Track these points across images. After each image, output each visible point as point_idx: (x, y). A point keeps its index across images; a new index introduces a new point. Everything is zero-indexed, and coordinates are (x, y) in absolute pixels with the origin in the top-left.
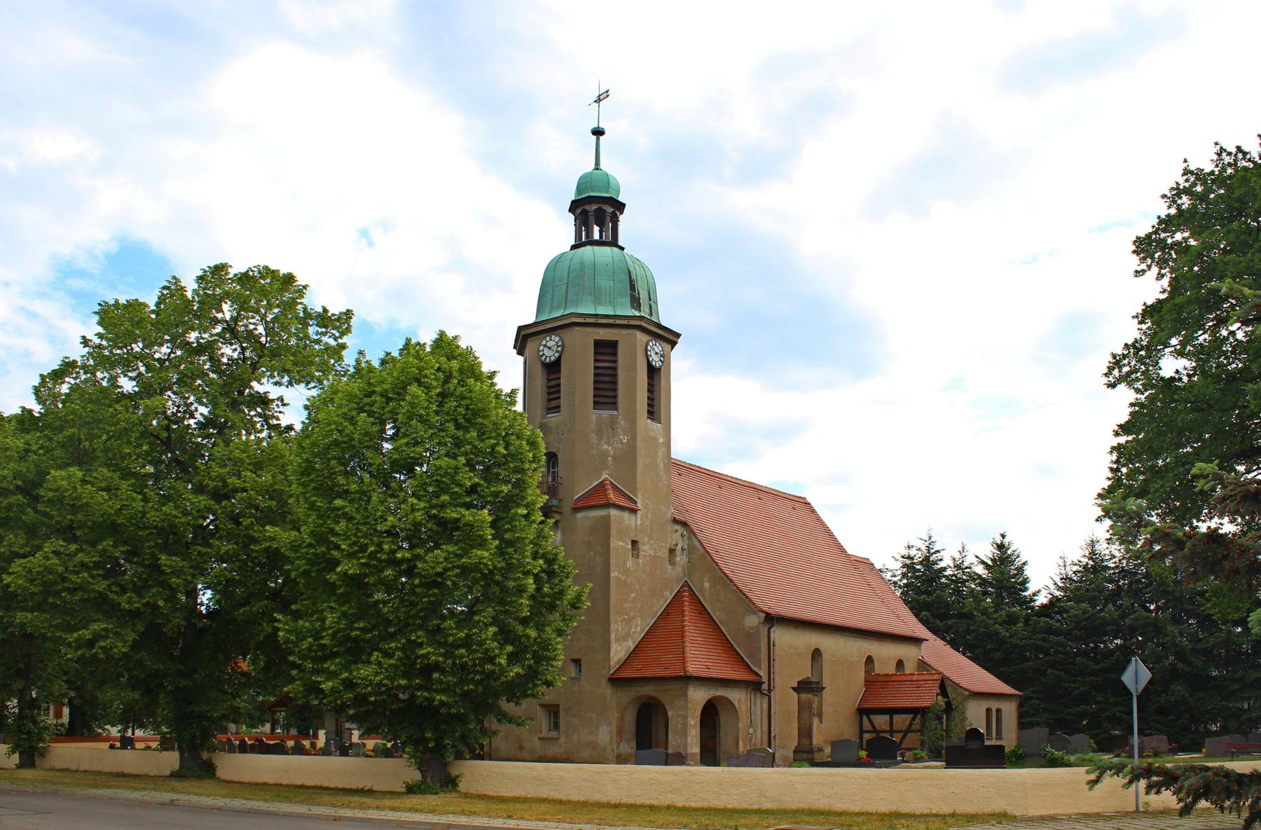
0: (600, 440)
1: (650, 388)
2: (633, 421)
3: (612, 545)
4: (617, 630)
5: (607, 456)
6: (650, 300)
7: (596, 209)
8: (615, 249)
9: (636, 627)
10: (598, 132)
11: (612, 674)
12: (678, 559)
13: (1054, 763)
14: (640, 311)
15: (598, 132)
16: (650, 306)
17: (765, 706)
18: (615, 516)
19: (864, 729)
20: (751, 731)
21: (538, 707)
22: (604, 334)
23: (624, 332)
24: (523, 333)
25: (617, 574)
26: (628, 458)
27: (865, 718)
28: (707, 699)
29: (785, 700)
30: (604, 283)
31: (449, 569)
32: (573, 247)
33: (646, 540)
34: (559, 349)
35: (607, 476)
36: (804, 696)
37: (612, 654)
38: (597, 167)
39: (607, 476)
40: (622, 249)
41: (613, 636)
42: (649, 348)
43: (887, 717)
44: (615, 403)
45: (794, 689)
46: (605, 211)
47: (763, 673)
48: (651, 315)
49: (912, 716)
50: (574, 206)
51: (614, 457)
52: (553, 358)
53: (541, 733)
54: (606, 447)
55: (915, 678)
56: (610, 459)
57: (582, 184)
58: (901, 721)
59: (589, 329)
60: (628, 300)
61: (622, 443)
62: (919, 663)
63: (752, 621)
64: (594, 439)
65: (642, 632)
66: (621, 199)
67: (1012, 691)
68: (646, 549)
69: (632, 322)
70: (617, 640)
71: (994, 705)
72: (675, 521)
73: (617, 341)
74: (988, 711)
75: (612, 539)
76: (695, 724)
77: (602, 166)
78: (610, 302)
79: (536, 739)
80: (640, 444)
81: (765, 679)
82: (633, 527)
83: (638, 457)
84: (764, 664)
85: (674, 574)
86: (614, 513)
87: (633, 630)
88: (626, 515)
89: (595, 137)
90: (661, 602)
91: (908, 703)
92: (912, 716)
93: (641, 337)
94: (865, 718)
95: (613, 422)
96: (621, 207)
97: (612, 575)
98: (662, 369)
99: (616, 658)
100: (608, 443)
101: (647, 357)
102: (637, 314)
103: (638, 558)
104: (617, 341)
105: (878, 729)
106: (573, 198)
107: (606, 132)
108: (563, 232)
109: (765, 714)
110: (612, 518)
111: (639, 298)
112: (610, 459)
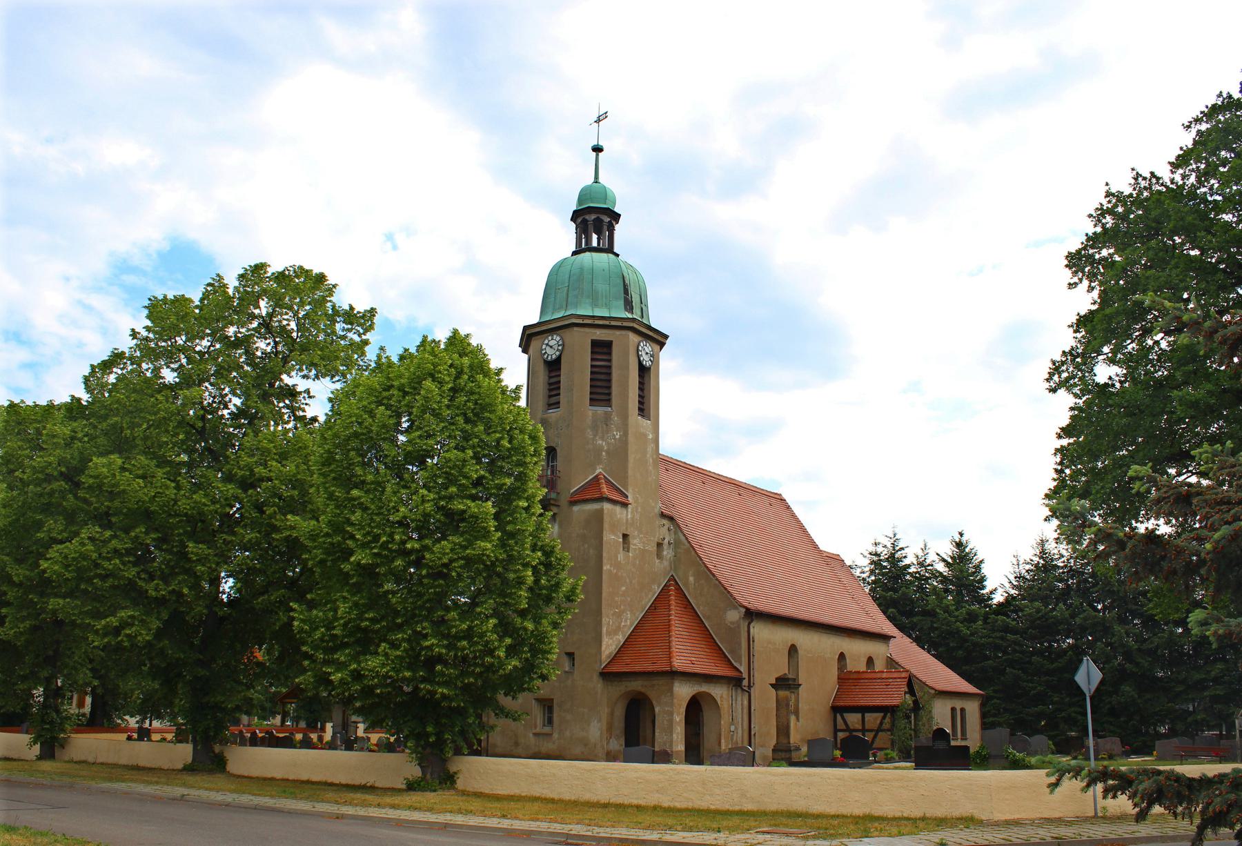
0: (595, 436)
1: (641, 406)
2: (625, 417)
3: (605, 539)
4: (608, 624)
8: (611, 256)
9: (626, 621)
10: (597, 149)
13: (1016, 765)
14: (632, 313)
15: (597, 149)
16: (642, 309)
17: (746, 702)
18: (608, 509)
20: (733, 728)
21: (534, 701)
23: (618, 333)
24: (528, 332)
26: (620, 453)
27: (838, 715)
29: (764, 697)
32: (574, 253)
34: (560, 348)
35: (601, 470)
36: (782, 693)
38: (596, 181)
39: (601, 470)
40: (617, 255)
41: (604, 630)
43: (859, 715)
46: (602, 221)
47: (744, 668)
48: (642, 317)
49: (882, 714)
50: (576, 216)
51: (608, 452)
52: (554, 357)
55: (884, 675)
56: (604, 453)
57: (584, 195)
59: (587, 330)
60: (622, 302)
61: (615, 439)
63: (734, 616)
65: (631, 625)
67: (975, 690)
68: (635, 543)
69: (625, 324)
71: (958, 704)
72: (663, 515)
74: (953, 709)
75: (604, 533)
76: (680, 720)
77: (601, 180)
79: (531, 735)
80: (631, 439)
81: (745, 675)
82: (625, 521)
84: (745, 660)
85: (661, 567)
90: (650, 596)
91: (879, 701)
92: (882, 714)
93: (633, 338)
94: (838, 715)
95: (607, 418)
97: (605, 568)
99: (607, 652)
101: (639, 357)
102: (630, 316)
105: (880, 733)
108: (564, 239)
109: (746, 711)
110: (605, 512)
112: (604, 453)
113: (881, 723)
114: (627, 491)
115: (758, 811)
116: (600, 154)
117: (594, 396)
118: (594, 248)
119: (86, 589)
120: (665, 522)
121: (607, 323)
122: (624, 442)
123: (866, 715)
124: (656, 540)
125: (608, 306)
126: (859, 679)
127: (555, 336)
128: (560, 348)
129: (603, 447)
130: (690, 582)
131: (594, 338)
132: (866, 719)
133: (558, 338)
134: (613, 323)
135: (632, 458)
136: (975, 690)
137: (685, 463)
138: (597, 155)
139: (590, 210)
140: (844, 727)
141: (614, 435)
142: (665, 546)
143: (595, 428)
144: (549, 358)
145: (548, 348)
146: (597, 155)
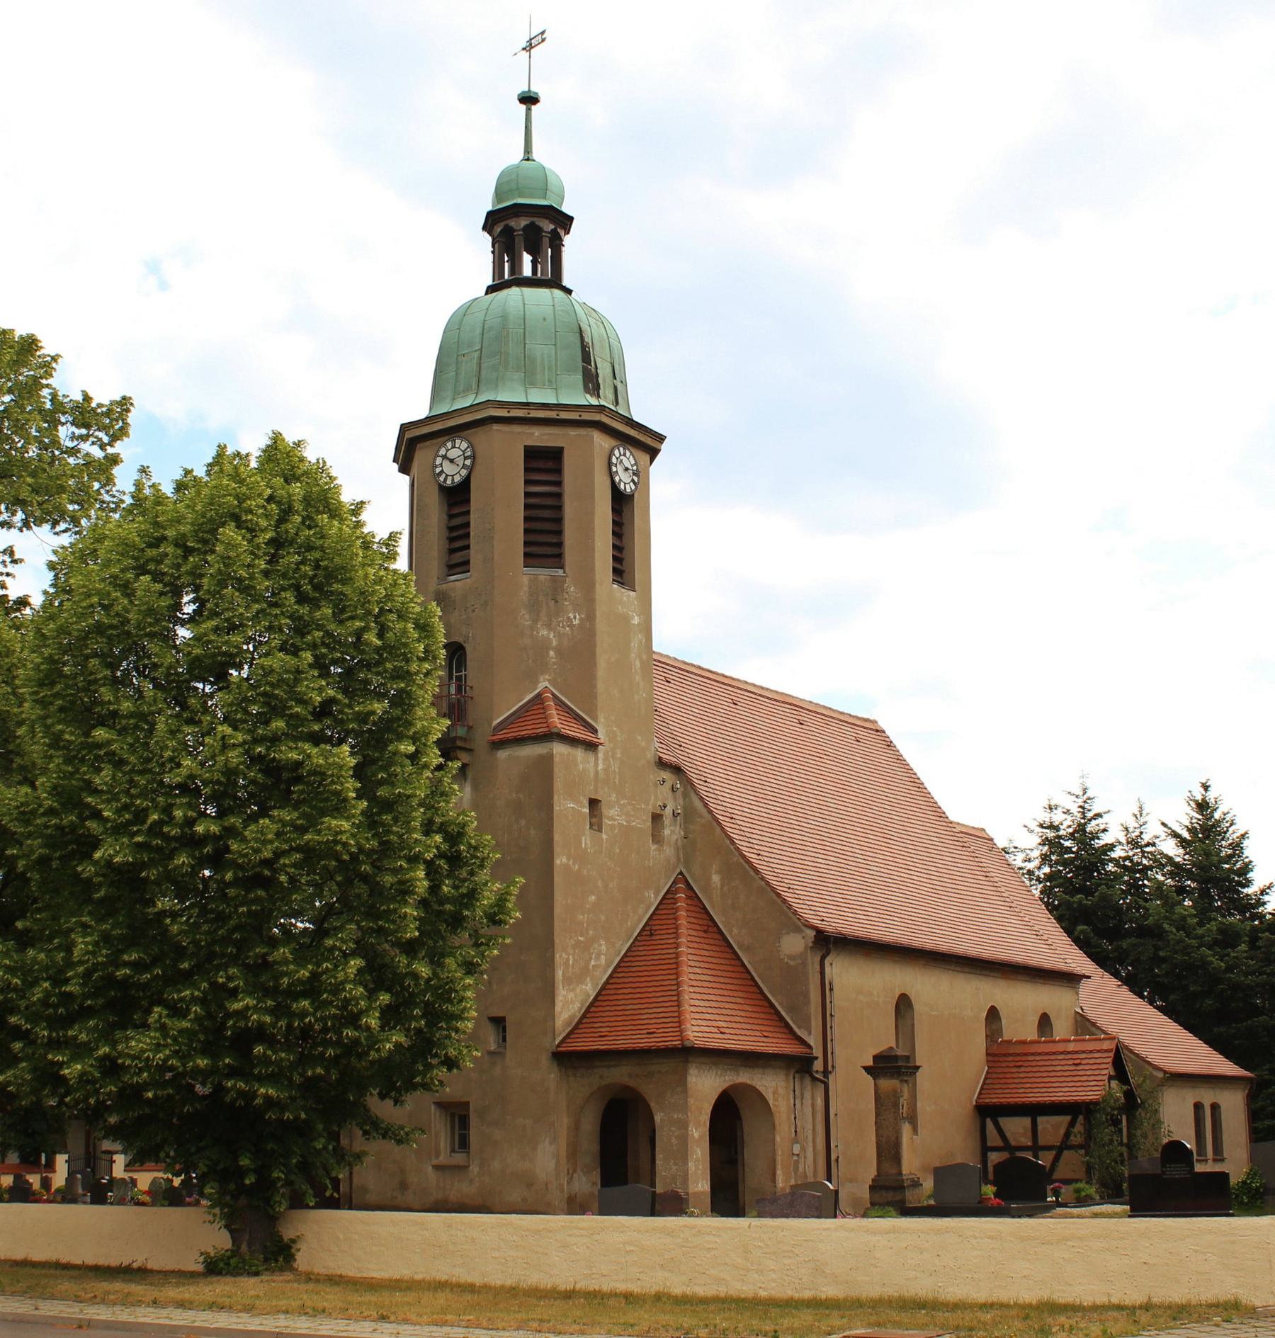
0: (535, 621)
2: (589, 587)
3: (556, 808)
6: (615, 378)
8: (557, 292)
10: (529, 100)
14: (599, 396)
15: (529, 100)
16: (616, 389)
17: (820, 1102)
21: (433, 1107)
22: (541, 437)
23: (573, 432)
25: (564, 860)
32: (491, 290)
33: (613, 797)
35: (547, 684)
39: (547, 684)
40: (569, 292)
41: (559, 974)
43: (1027, 1121)
44: (560, 556)
45: (868, 1069)
47: (814, 1040)
48: (617, 403)
50: (492, 221)
51: (558, 650)
53: (437, 1156)
56: (552, 653)
58: (1052, 1127)
59: (517, 429)
61: (571, 626)
62: (1076, 1021)
63: (794, 944)
64: (525, 618)
66: (566, 209)
69: (587, 416)
71: (1207, 1096)
74: (1198, 1107)
75: (556, 797)
76: (701, 1137)
77: (536, 155)
78: (550, 381)
80: (601, 626)
81: (818, 1052)
82: (592, 775)
83: (598, 650)
86: (559, 749)
87: (593, 963)
88: (579, 753)
89: (524, 107)
90: (640, 911)
95: (556, 588)
98: (636, 495)
100: (549, 626)
101: (611, 475)
102: (594, 401)
103: (600, 830)
104: (563, 448)
106: (490, 208)
107: (542, 100)
110: (557, 759)
111: (597, 375)
112: (552, 653)
113: (1067, 1135)
114: (596, 722)
116: (533, 107)
120: (666, 775)
123: (1040, 1119)
125: (553, 384)
126: (1026, 1054)
127: (458, 442)
128: (468, 462)
132: (1040, 1128)
133: (464, 445)
134: (564, 415)
138: (529, 111)
139: (518, 210)
144: (449, 482)
146: (529, 111)
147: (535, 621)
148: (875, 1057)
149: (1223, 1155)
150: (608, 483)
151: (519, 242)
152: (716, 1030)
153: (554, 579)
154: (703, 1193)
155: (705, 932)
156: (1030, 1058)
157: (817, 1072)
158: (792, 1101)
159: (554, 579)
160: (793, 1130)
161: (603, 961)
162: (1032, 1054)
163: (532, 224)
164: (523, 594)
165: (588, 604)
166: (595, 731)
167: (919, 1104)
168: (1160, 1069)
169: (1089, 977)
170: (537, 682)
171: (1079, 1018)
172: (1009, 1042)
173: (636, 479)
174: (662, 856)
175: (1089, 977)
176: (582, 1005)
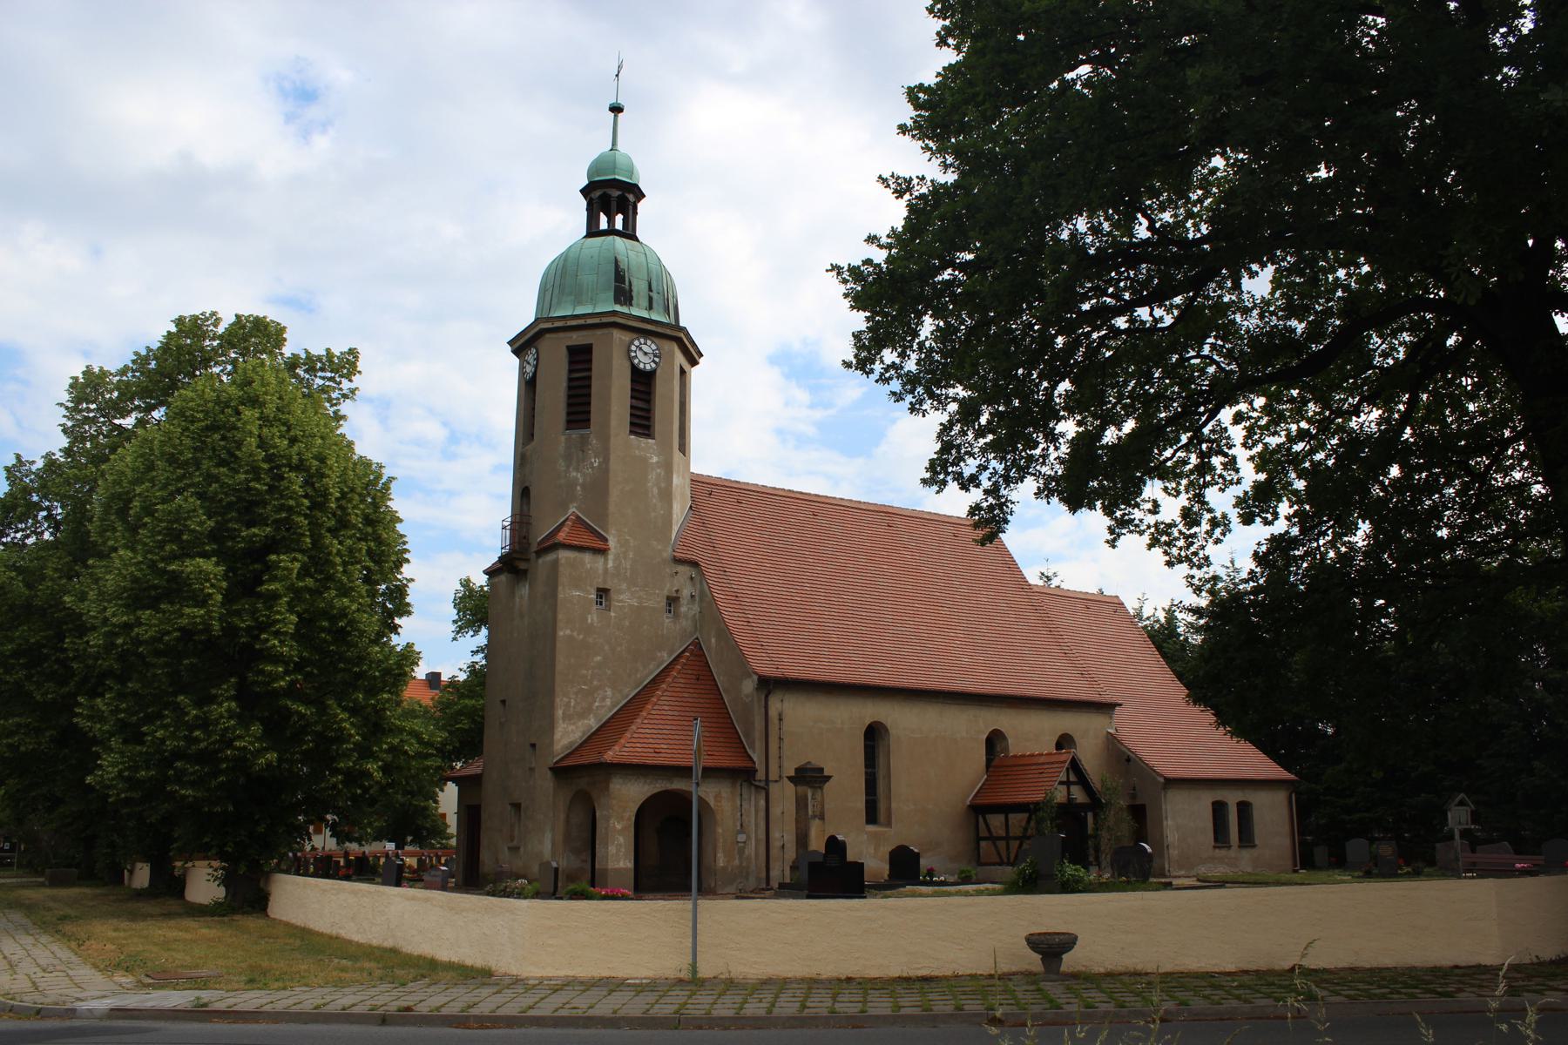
0: (568, 467)
2: (605, 439)
3: (561, 596)
4: (568, 705)
5: (576, 485)
6: (650, 289)
7: (600, 197)
9: (603, 699)
10: (616, 109)
11: (556, 763)
12: (683, 609)
13: (1068, 887)
14: (631, 305)
15: (616, 109)
16: (651, 299)
17: (762, 803)
18: (566, 558)
19: (981, 835)
20: (741, 838)
21: (509, 807)
22: (577, 339)
23: (599, 332)
25: (568, 632)
26: (599, 488)
28: (649, 794)
30: (587, 279)
31: (168, 633)
33: (624, 586)
35: (574, 510)
36: (800, 789)
37: (558, 735)
39: (574, 510)
41: (560, 713)
42: (633, 348)
43: (1001, 817)
46: (610, 196)
47: (757, 756)
48: (650, 307)
51: (583, 486)
52: (648, 367)
53: (512, 840)
54: (575, 474)
56: (579, 488)
57: (594, 169)
58: (1017, 819)
59: (561, 335)
60: (611, 294)
61: (593, 468)
62: (1108, 739)
63: (749, 686)
64: (561, 465)
65: (615, 706)
67: (1285, 775)
68: (624, 598)
69: (605, 320)
70: (567, 717)
71: (1232, 798)
72: (678, 561)
73: (592, 344)
74: (1219, 809)
75: (560, 588)
76: (624, 829)
77: (620, 147)
78: (592, 299)
79: (506, 849)
80: (614, 465)
82: (600, 571)
83: (611, 483)
84: (759, 745)
85: (674, 632)
86: (564, 555)
87: (597, 704)
88: (587, 558)
90: (651, 667)
91: (1022, 798)
93: (618, 335)
95: (584, 442)
96: (640, 195)
97: (561, 633)
98: (658, 372)
99: (565, 742)
100: (577, 470)
101: (631, 359)
103: (608, 608)
104: (592, 344)
105: (995, 834)
109: (762, 814)
110: (563, 561)
111: (631, 290)
112: (579, 488)
113: (1026, 829)
114: (607, 533)
115: (458, 964)
117: (573, 417)
118: (618, 230)
119: (312, 672)
120: (681, 568)
121: (581, 322)
122: (605, 470)
123: (1011, 816)
124: (666, 592)
125: (593, 301)
127: (649, 342)
129: (577, 479)
130: (711, 643)
131: (570, 343)
132: (1010, 823)
133: (654, 347)
134: (590, 321)
135: (615, 493)
136: (1285, 775)
137: (801, 493)
140: (987, 834)
141: (592, 463)
142: (684, 601)
143: (568, 457)
145: (639, 354)
147: (568, 467)
148: (796, 769)
149: (1254, 842)
150: (628, 365)
151: (614, 205)
152: (652, 750)
153: (582, 436)
154: (626, 869)
155: (698, 679)
156: (1015, 769)
157: (760, 781)
158: (739, 803)
159: (582, 436)
160: (739, 824)
161: (608, 702)
162: (1035, 764)
163: (604, 193)
164: (561, 448)
165: (605, 454)
166: (606, 540)
167: (894, 805)
168: (1162, 776)
169: (1120, 705)
170: (568, 509)
171: (1110, 737)
172: (1015, 756)
173: (657, 360)
174: (678, 627)
175: (1120, 705)
176: (584, 734)
